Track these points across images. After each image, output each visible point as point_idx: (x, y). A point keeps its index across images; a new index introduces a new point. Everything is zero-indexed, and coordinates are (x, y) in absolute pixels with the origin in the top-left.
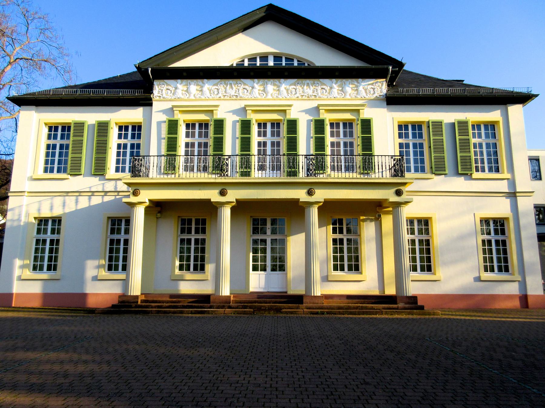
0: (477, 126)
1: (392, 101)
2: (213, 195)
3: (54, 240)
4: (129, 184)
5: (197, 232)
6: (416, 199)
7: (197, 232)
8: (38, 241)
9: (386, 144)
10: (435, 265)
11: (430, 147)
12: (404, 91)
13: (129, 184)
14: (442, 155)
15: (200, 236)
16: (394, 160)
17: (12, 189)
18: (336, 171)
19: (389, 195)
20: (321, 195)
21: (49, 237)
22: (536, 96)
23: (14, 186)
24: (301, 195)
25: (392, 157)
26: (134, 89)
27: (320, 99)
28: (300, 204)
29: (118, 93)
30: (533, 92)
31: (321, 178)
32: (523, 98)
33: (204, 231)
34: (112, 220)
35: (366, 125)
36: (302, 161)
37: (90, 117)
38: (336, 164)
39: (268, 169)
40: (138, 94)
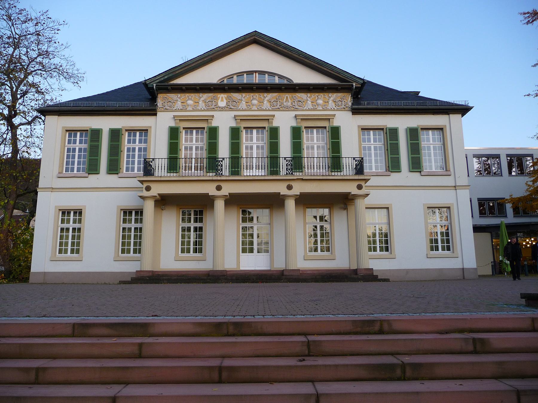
0: (132, 131)
1: (355, 111)
2: (210, 189)
3: (75, 228)
4: (142, 182)
5: (196, 221)
6: (372, 192)
7: (196, 221)
8: (62, 229)
9: (350, 149)
10: (206, 249)
11: (387, 150)
12: (365, 105)
13: (142, 182)
14: (392, 156)
15: (138, 225)
16: (287, 161)
17: (40, 185)
18: (199, 171)
19: (351, 188)
20: (298, 188)
21: (133, 225)
22: (471, 108)
23: (41, 184)
24: (281, 189)
25: (354, 158)
26: (143, 98)
27: (296, 110)
28: (281, 197)
29: (368, 104)
30: (470, 105)
31: (298, 175)
32: (463, 110)
33: (201, 221)
34: (124, 212)
35: (335, 132)
36: (283, 163)
37: (105, 124)
38: (260, 164)
39: (254, 169)
40: (145, 105)
